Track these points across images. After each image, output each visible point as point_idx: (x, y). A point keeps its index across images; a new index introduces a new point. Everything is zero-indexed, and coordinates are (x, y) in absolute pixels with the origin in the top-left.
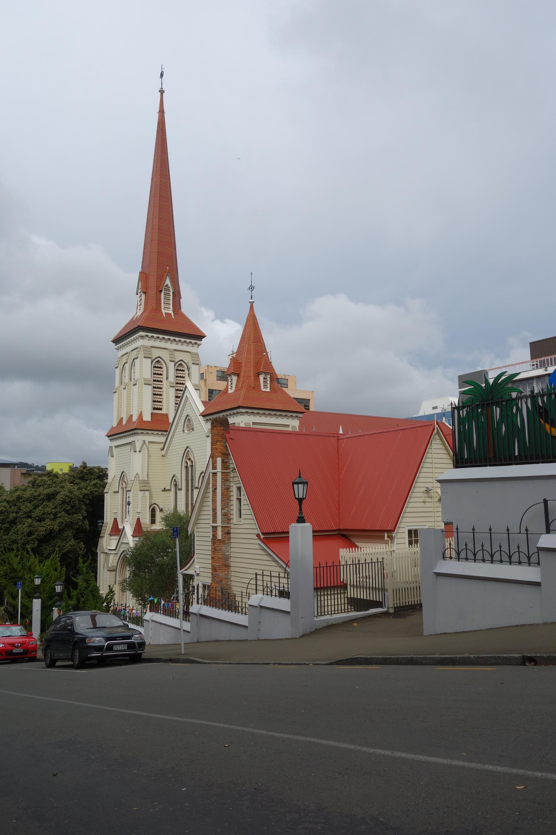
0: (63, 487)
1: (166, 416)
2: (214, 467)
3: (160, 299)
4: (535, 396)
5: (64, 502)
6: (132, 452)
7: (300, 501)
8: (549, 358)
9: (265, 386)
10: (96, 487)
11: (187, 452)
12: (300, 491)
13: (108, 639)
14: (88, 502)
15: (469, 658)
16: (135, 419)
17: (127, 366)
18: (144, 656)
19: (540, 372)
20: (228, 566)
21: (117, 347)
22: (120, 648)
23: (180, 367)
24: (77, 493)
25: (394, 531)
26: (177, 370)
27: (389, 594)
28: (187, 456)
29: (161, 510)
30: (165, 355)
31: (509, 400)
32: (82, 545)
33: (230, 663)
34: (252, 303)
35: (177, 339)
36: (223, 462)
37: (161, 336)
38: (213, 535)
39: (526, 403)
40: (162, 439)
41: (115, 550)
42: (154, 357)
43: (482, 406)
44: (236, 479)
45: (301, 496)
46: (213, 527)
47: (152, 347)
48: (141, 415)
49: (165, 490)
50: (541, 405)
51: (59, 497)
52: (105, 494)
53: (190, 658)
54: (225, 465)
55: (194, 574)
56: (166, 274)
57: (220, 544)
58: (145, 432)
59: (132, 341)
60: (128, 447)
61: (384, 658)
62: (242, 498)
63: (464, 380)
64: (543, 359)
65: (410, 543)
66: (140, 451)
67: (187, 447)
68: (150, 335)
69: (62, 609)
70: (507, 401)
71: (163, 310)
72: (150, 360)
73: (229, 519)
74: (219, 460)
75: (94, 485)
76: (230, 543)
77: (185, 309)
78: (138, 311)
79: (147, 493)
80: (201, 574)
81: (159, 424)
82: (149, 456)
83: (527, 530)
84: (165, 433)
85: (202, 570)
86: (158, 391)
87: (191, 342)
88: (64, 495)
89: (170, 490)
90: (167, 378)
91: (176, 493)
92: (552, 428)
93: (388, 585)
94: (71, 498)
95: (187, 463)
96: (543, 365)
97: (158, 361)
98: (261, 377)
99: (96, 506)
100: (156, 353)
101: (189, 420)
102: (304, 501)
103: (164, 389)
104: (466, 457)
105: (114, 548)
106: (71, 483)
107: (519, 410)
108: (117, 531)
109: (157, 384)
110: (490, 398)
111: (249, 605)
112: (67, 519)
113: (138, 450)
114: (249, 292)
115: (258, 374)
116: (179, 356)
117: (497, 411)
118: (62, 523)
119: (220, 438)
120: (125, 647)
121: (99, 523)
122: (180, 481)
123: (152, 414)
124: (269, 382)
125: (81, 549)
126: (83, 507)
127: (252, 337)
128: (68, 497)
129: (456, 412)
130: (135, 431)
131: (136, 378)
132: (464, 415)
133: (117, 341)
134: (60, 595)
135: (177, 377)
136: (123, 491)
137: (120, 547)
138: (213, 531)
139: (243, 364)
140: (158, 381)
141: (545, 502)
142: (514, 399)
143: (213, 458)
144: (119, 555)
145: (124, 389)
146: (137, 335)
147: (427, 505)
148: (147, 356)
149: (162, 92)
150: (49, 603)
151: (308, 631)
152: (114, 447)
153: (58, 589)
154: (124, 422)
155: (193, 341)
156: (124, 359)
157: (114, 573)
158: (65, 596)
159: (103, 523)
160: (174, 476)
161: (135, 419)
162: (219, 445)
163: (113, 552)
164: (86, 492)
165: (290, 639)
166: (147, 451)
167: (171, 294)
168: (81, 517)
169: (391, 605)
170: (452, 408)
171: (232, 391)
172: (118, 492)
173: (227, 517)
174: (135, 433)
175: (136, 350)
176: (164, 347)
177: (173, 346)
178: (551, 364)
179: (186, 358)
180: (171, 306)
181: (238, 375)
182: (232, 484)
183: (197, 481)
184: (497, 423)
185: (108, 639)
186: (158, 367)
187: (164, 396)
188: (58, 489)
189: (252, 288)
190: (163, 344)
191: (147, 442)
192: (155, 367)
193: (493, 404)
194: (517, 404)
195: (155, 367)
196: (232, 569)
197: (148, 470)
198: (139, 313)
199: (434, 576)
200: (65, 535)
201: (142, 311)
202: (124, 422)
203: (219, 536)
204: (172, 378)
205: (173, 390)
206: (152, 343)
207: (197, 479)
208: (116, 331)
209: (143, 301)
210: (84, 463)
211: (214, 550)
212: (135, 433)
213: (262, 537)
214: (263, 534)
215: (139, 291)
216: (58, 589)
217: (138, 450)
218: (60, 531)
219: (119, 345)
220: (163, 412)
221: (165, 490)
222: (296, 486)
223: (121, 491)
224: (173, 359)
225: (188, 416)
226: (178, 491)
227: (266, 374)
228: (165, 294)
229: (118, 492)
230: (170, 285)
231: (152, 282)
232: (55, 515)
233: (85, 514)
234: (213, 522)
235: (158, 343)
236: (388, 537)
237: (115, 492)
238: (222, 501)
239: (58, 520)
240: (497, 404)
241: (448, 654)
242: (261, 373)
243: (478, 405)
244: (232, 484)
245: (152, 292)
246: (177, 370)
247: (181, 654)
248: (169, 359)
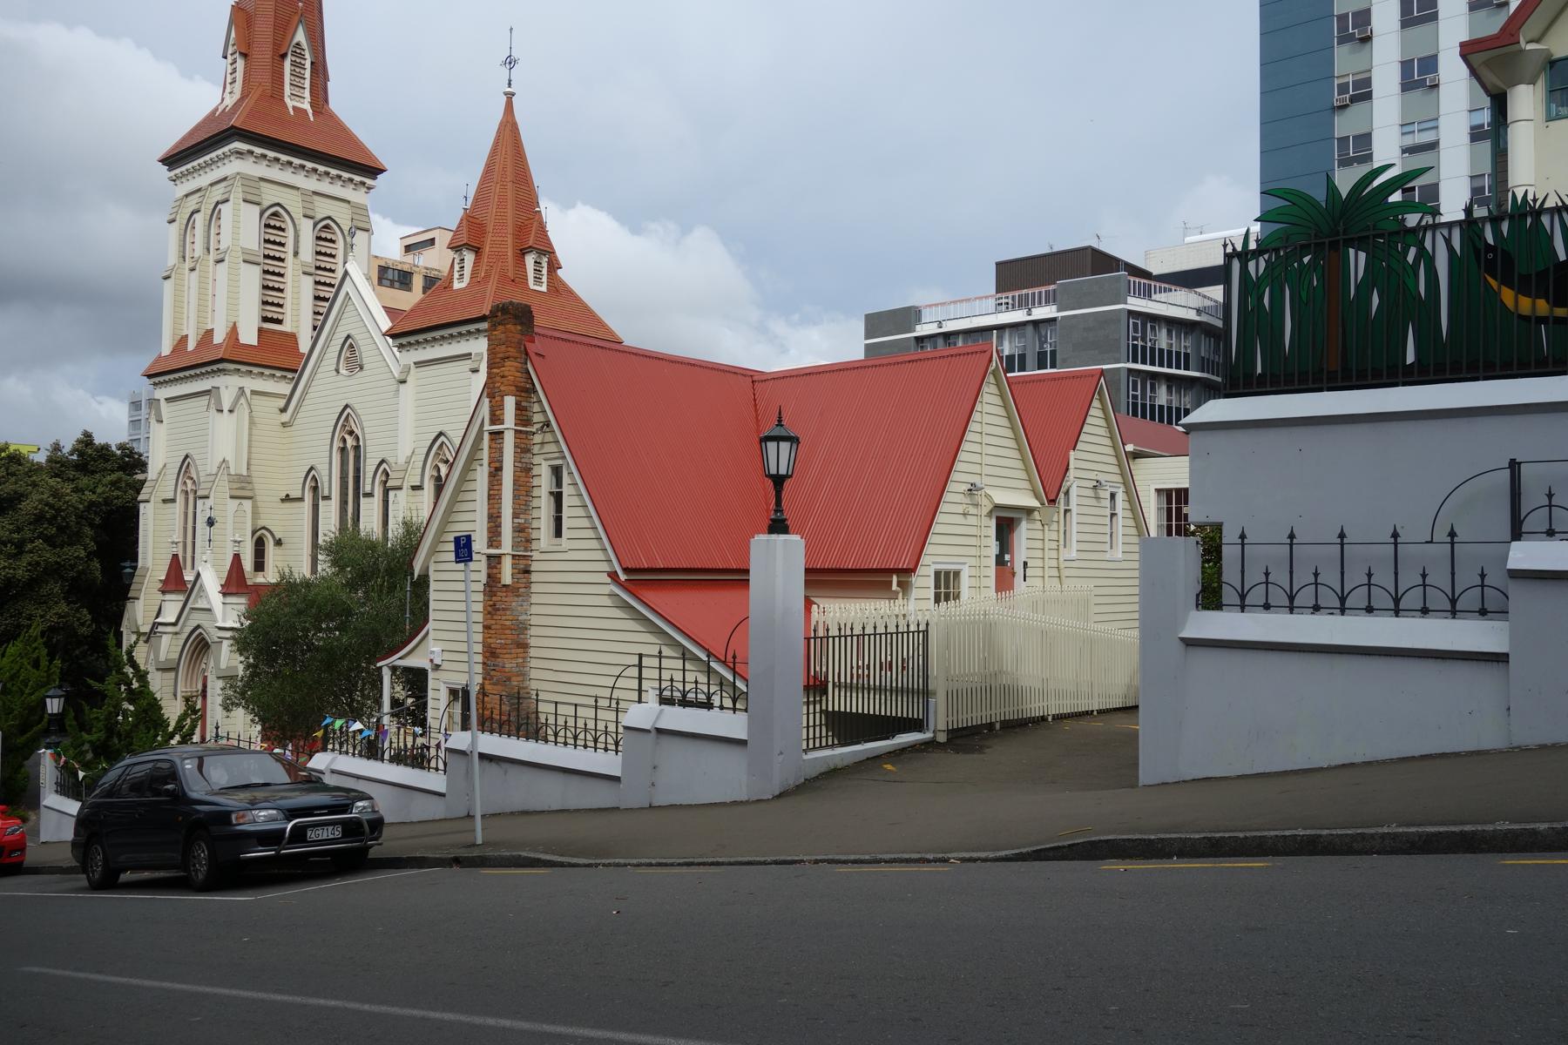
0: (34, 485)
1: (293, 337)
2: (496, 418)
3: (282, 75)
4: (1475, 221)
5: (39, 518)
6: (213, 411)
7: (779, 481)
8: (1037, 290)
9: (538, 280)
10: (118, 489)
11: (345, 421)
12: (780, 457)
13: (292, 813)
14: (98, 520)
15: (1534, 832)
16: (219, 338)
17: (199, 219)
18: (32, 856)
19: (1019, 316)
20: (525, 646)
21: (172, 174)
22: (325, 835)
23: (325, 232)
24: (74, 498)
25: (914, 570)
26: (319, 238)
27: (939, 704)
28: (344, 426)
29: (278, 543)
30: (293, 202)
31: (1397, 233)
32: (86, 615)
33: (659, 865)
34: (510, 96)
35: (321, 168)
36: (519, 407)
37: (284, 158)
38: (489, 576)
39: (1448, 241)
40: (285, 388)
42: (266, 204)
43: (1317, 249)
44: (548, 448)
45: (783, 471)
46: (489, 557)
47: (262, 179)
49: (287, 499)
50: (1490, 241)
51: (28, 506)
52: (142, 506)
53: (524, 854)
54: (523, 416)
55: (428, 666)
56: (296, 18)
57: (503, 601)
58: (244, 368)
59: (213, 162)
60: (204, 400)
61: (1209, 839)
62: (567, 490)
63: (876, 323)
65: (937, 600)
67: (347, 406)
68: (258, 151)
69: (65, 751)
70: (1391, 234)
71: (287, 100)
72: (257, 209)
73: (529, 541)
74: (510, 403)
75: (113, 483)
76: (529, 595)
77: (336, 103)
78: (227, 95)
79: (247, 504)
80: (445, 666)
81: (276, 355)
82: (252, 423)
83: (1452, 534)
84: (290, 375)
85: (447, 656)
86: (273, 281)
87: (351, 180)
88: (40, 501)
89: (301, 499)
90: (296, 254)
91: (316, 507)
92: (1521, 297)
93: (937, 683)
94: (59, 510)
95: (344, 441)
96: (1023, 303)
97: (275, 214)
98: (530, 260)
99: (118, 531)
100: (270, 195)
101: (351, 346)
102: (787, 483)
103: (289, 278)
104: (1259, 370)
106: (57, 476)
107: (1428, 258)
108: (175, 581)
109: (273, 266)
110: (1341, 229)
111: (626, 728)
112: (49, 556)
113: (226, 408)
115: (523, 253)
116: (323, 208)
117: (1358, 261)
118: (38, 564)
119: (512, 352)
120: (338, 833)
122: (326, 479)
123: (260, 330)
124: (545, 271)
125: (83, 624)
126: (88, 531)
127: (509, 170)
128: (51, 506)
129: (1236, 265)
130: (220, 366)
131: (223, 247)
132: (1261, 271)
133: (172, 160)
134: (58, 719)
135: (318, 253)
136: (187, 500)
137: (187, 619)
138: (490, 567)
139: (490, 228)
140: (274, 258)
141: (1514, 466)
142: (1413, 231)
143: (491, 396)
144: (185, 636)
145: (193, 270)
146: (226, 149)
147: (972, 520)
148: (250, 197)
150: (21, 740)
151: (792, 783)
152: (163, 402)
153: (54, 706)
154: (191, 346)
155: (357, 178)
156: (192, 203)
157: (172, 674)
158: (70, 722)
159: (135, 568)
160: (312, 468)
161: (219, 338)
162: (510, 368)
163: (170, 629)
164: (94, 497)
165: (747, 803)
166: (247, 411)
167: (308, 65)
168: (83, 554)
169: (942, 726)
170: (1226, 255)
171: (463, 285)
172: (173, 501)
173: (523, 534)
174: (219, 370)
176: (295, 184)
177: (312, 184)
179: (343, 216)
180: (307, 94)
181: (477, 251)
182: (536, 460)
183: (369, 481)
184: (1357, 287)
185: (292, 813)
186: (274, 227)
187: (288, 293)
188: (21, 487)
189: (510, 62)
190: (287, 176)
191: (248, 393)
192: (268, 226)
193: (1349, 243)
194: (1422, 242)
195: (268, 226)
196: (532, 652)
197: (249, 453)
198: (230, 102)
199: (1181, 646)
200: (43, 592)
201: (237, 96)
202: (191, 346)
203: (507, 577)
204: (307, 254)
205: (309, 280)
206: (261, 170)
207: (369, 475)
208: (167, 144)
209: (239, 75)
210: (87, 435)
211: (492, 610)
212: (219, 370)
213: (623, 577)
214: (626, 570)
215: (230, 51)
216: (54, 706)
217: (226, 408)
218: (33, 583)
219: (178, 171)
220: (286, 327)
221: (287, 499)
222: (772, 446)
223: (180, 498)
224: (310, 213)
225: (348, 337)
226: (321, 503)
227: (541, 253)
228: (293, 63)
230: (304, 45)
231: (264, 31)
232: (20, 546)
233: (93, 546)
234: (490, 546)
235: (275, 173)
236: (899, 584)
237: (165, 501)
238: (514, 497)
239: (26, 558)
240: (1360, 243)
241: (1455, 824)
242: (530, 249)
243: (1302, 246)
244: (536, 460)
245: (263, 54)
246: (319, 238)
247: (474, 845)
248: (301, 211)
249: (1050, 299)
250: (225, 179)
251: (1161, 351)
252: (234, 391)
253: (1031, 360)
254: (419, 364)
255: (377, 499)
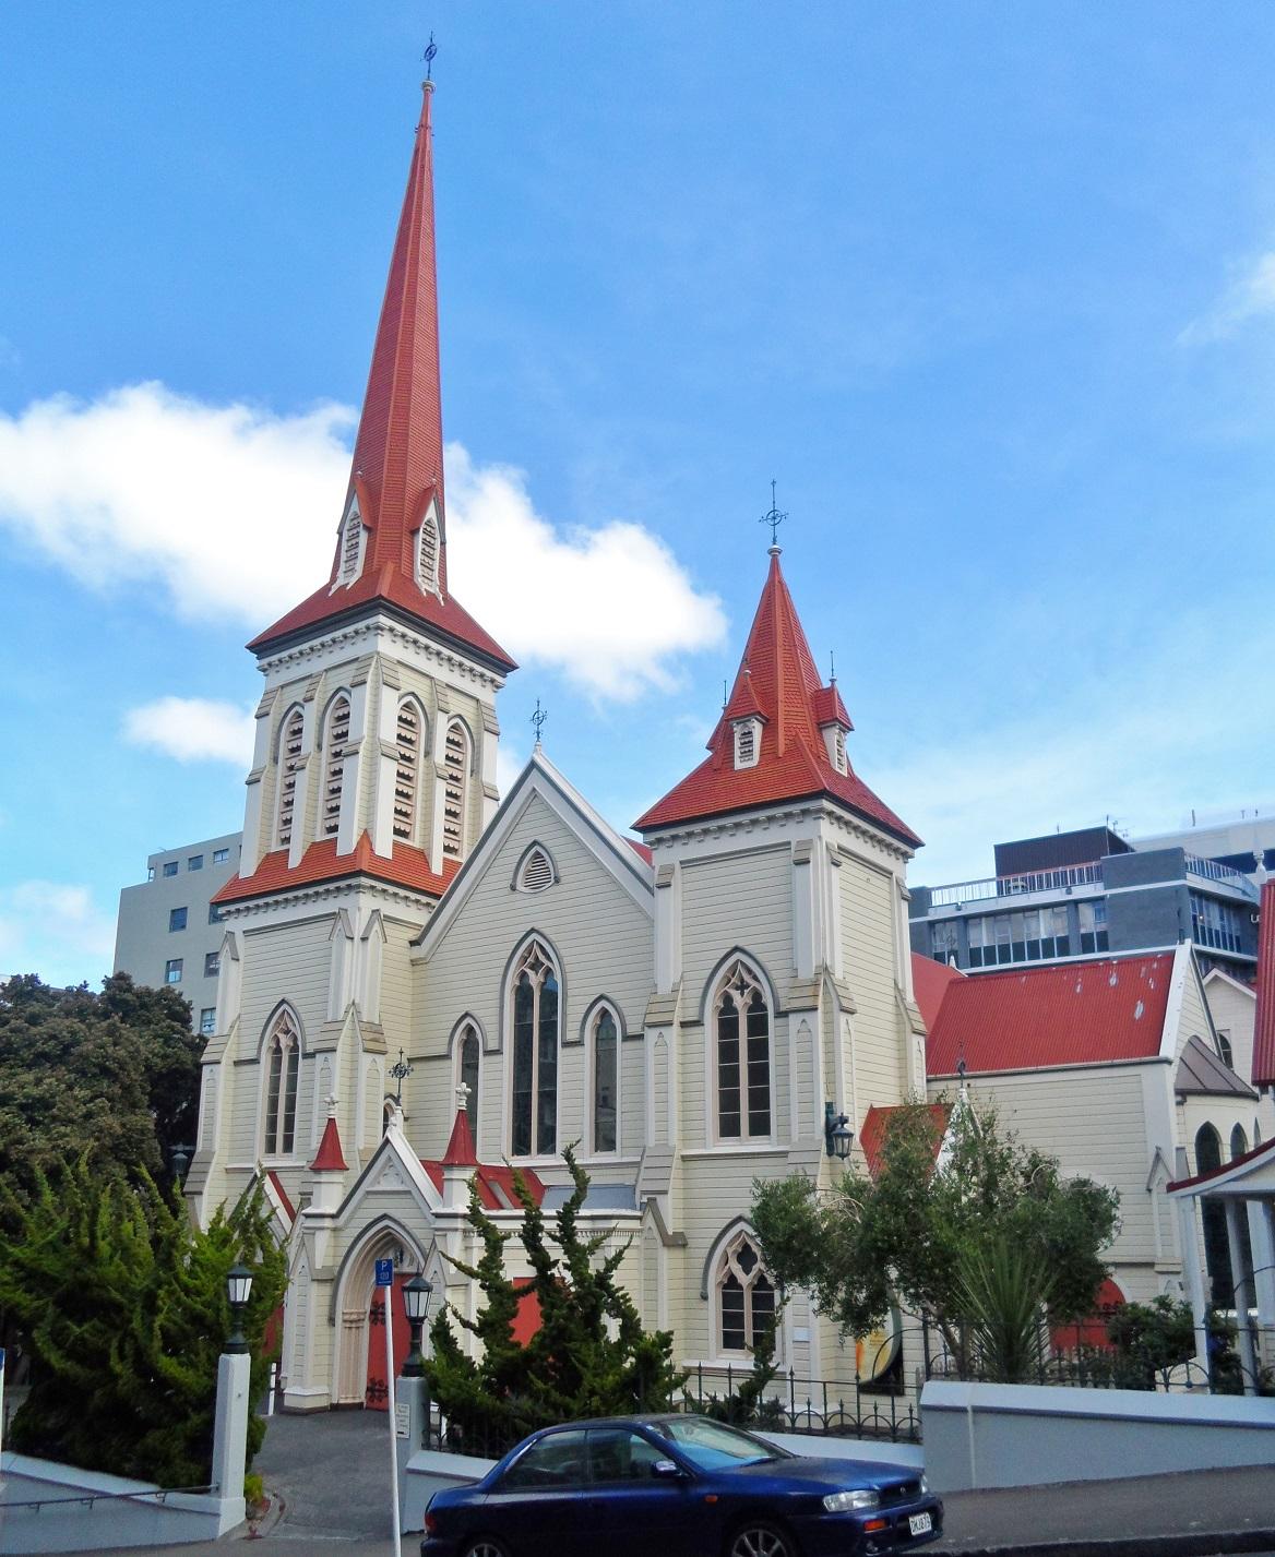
28: (277, 1023)
40: (420, 917)
41: (332, 1217)
48: (366, 838)
52: (206, 1070)
60: (326, 926)
64: (1060, 869)
66: (364, 939)
72: (396, 694)
90: (427, 754)
105: (333, 1211)
113: (357, 936)
114: (767, 529)
121: (177, 1152)
130: (353, 882)
149: (427, 89)
154: (294, 861)
159: (191, 1154)
163: (328, 1223)
175: (355, 665)
178: (1081, 880)
189: (775, 517)
204: (441, 750)
215: (347, 527)
217: (357, 936)
229: (255, 1061)
249: (1097, 876)
250: (357, 659)
251: (1217, 932)
252: (366, 914)
253: (1074, 943)
254: (685, 864)
255: (587, 1052)
